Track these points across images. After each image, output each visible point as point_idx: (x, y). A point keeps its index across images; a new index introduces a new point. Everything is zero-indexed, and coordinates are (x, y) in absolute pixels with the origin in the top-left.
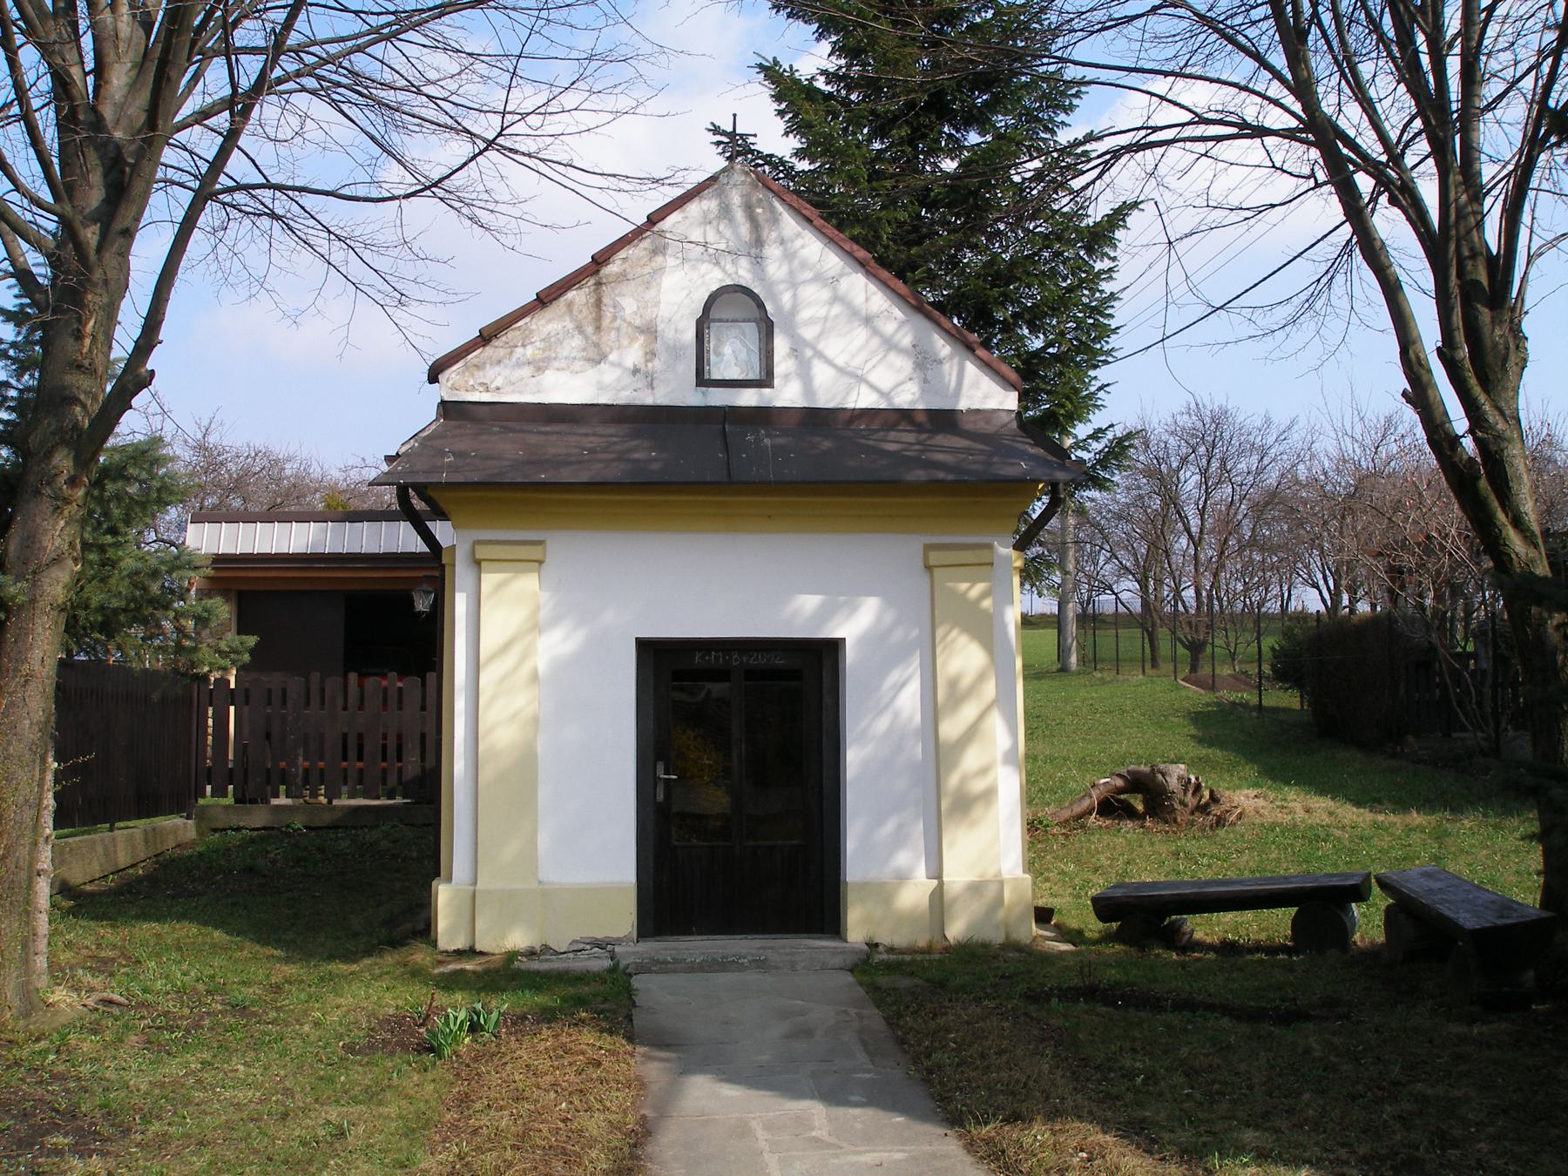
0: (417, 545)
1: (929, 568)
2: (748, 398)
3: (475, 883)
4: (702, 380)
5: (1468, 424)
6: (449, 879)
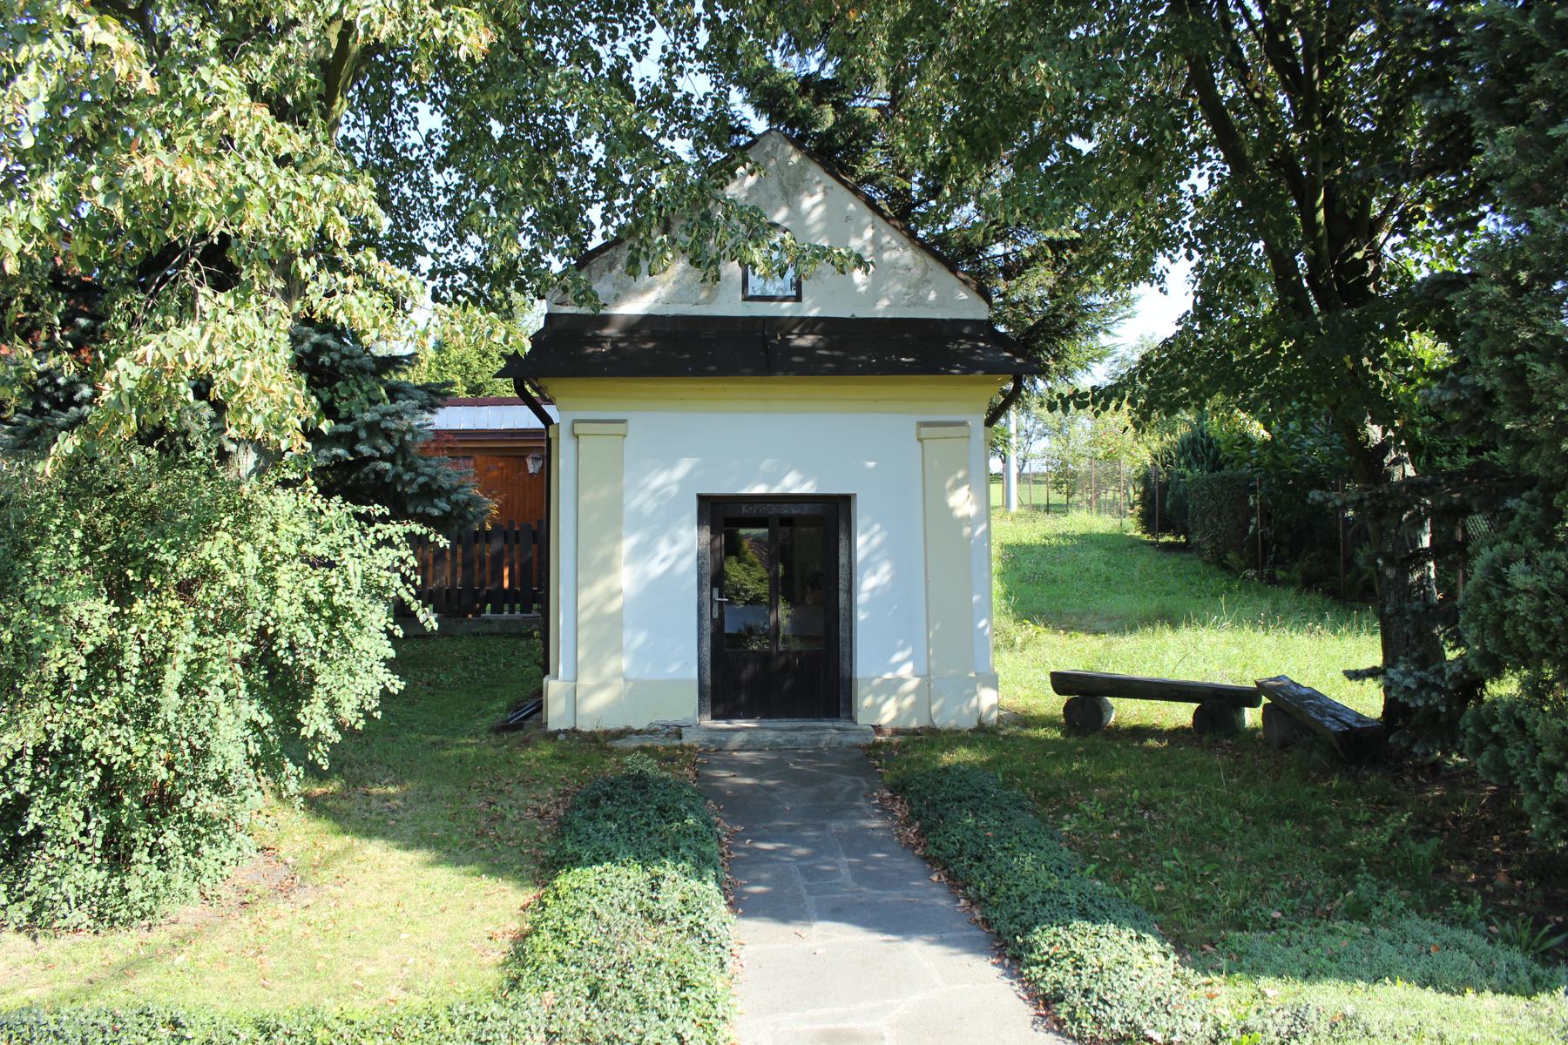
1: (920, 440)
2: (786, 309)
4: (747, 298)
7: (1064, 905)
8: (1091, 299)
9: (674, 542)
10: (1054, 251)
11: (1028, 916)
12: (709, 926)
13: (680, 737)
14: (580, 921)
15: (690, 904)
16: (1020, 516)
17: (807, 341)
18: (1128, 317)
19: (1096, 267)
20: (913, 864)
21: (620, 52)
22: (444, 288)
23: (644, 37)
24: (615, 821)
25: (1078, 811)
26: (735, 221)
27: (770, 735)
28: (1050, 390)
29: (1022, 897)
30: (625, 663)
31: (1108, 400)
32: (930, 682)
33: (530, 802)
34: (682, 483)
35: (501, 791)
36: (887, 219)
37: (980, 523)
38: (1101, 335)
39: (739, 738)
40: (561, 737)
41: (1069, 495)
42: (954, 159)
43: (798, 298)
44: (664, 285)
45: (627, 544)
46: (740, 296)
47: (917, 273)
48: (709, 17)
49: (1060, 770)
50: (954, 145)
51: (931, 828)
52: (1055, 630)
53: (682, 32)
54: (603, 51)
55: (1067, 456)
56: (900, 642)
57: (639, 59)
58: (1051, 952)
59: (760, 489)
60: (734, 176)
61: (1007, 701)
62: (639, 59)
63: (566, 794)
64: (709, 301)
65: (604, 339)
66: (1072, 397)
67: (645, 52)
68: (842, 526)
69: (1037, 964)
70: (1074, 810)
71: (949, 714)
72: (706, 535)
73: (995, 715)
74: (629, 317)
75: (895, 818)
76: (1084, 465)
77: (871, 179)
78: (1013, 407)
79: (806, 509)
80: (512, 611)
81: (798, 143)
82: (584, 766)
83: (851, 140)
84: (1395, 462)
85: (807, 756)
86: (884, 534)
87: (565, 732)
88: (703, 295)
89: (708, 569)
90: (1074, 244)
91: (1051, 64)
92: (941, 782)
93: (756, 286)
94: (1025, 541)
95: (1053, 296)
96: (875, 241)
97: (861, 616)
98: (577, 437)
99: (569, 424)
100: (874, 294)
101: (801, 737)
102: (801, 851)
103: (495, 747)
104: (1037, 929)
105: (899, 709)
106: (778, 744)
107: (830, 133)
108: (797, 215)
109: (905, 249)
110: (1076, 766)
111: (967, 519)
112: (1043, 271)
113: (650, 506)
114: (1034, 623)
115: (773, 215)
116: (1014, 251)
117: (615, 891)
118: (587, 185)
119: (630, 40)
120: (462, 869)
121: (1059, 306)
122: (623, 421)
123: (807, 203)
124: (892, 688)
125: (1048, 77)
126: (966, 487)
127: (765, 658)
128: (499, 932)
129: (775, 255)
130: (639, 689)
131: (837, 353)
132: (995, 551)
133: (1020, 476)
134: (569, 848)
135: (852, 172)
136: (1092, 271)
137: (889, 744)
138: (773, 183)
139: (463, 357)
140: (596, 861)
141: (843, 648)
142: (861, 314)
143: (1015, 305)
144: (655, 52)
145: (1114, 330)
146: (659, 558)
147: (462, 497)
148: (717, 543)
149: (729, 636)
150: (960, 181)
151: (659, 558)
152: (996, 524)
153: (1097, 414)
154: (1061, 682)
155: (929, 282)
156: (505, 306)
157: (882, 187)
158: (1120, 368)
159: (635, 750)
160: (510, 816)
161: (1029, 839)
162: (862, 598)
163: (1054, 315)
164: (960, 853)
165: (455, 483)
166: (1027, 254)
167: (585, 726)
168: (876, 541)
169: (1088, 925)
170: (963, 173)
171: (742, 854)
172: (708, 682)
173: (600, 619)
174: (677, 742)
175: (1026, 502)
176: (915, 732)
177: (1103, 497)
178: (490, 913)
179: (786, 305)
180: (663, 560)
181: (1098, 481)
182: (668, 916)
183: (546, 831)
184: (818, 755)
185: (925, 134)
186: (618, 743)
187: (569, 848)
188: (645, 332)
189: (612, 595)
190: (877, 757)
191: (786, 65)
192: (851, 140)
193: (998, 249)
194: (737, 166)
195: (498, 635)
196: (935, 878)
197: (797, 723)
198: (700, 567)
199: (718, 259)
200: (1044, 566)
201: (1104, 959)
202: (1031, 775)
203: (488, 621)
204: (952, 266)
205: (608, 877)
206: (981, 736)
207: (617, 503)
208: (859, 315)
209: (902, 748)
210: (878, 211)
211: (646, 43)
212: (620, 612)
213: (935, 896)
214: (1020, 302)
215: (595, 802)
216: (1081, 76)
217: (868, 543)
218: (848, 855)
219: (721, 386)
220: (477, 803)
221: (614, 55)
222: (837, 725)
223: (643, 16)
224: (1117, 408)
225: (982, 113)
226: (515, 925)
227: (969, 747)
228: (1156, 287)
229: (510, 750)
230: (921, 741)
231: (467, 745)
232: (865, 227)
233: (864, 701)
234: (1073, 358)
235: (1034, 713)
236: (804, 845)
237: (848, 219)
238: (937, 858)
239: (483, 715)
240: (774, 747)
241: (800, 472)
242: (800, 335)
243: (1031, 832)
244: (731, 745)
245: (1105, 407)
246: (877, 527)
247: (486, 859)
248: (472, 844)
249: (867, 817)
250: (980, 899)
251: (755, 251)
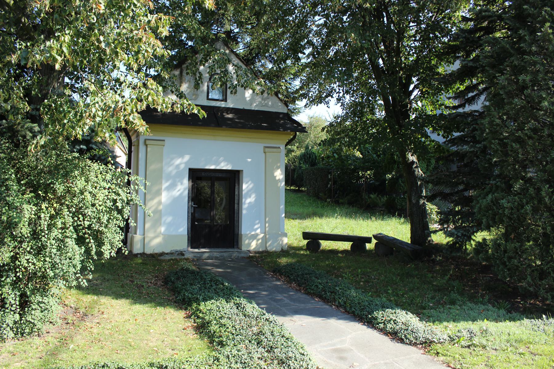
1: (265, 152)
2: (223, 104)
3: (144, 235)
17: (230, 116)
34: (186, 163)
39: (206, 255)
40: (139, 256)
51: (146, 264)
59: (213, 167)
68: (237, 181)
71: (272, 247)
84: (416, 167)
87: (140, 254)
97: (244, 212)
98: (146, 145)
101: (225, 255)
122: (164, 140)
124: (255, 237)
130: (167, 238)
131: (242, 121)
141: (236, 223)
142: (247, 108)
154: (306, 235)
167: (148, 251)
174: (183, 257)
180: (179, 191)
186: (162, 258)
207: (161, 170)
208: (246, 108)
228: (326, 105)
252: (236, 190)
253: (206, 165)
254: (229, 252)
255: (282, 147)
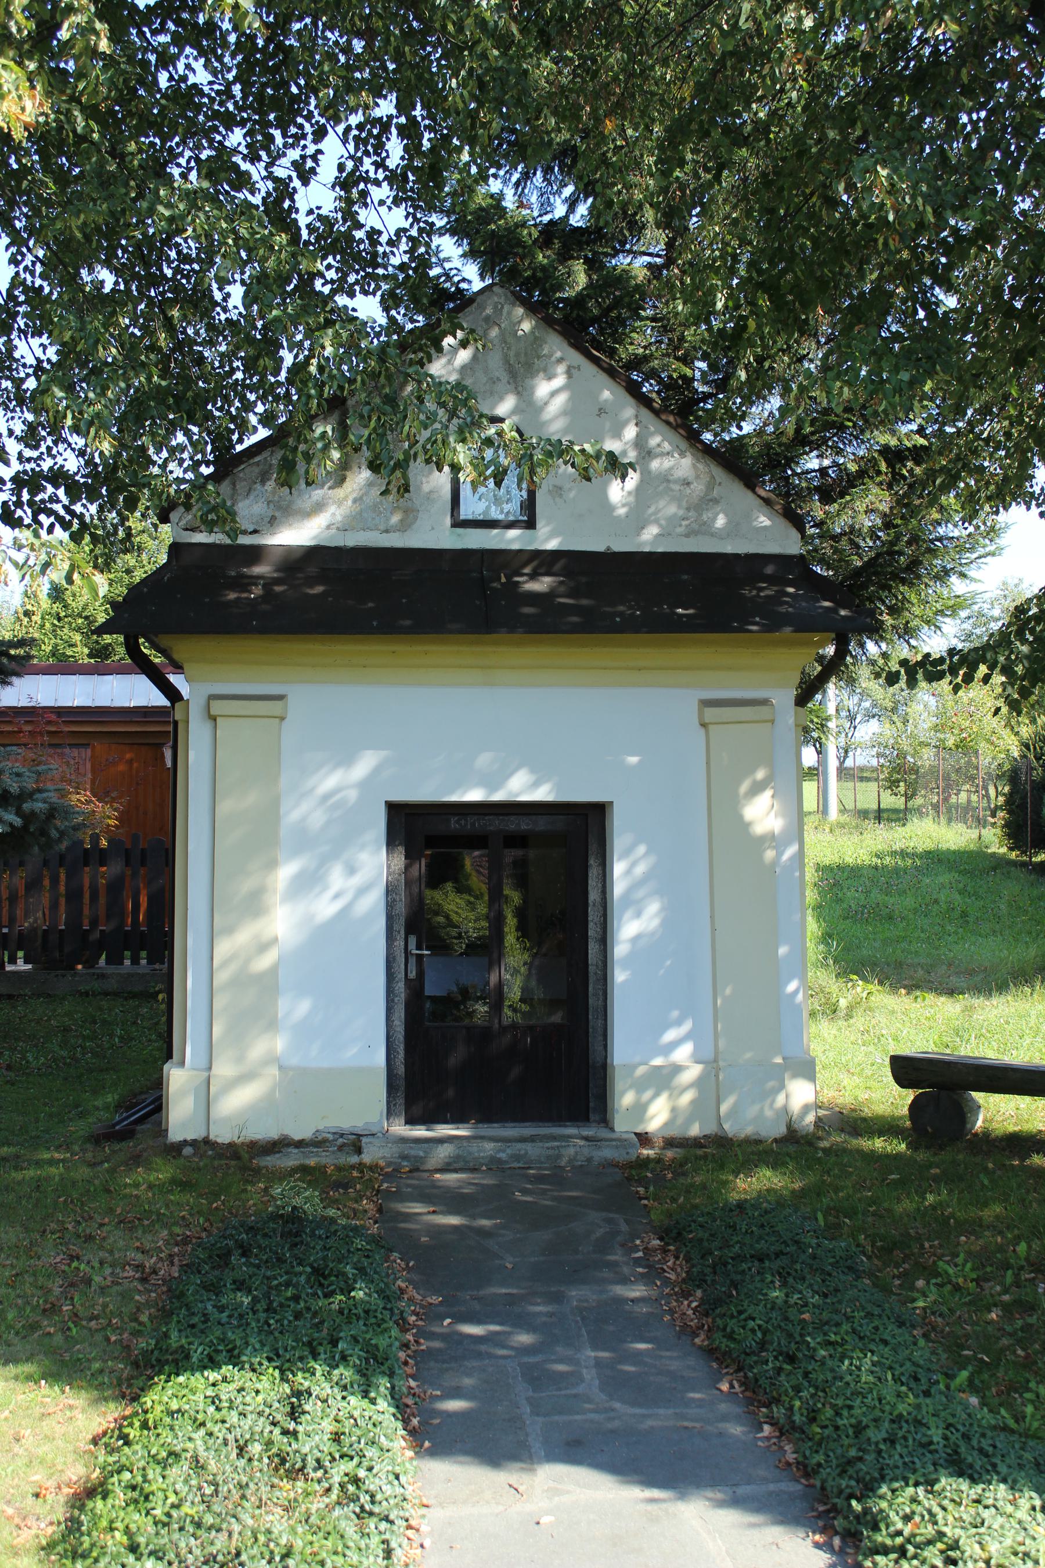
0: (159, 700)
1: (704, 725)
2: (513, 539)
3: (210, 1068)
4: (459, 523)
5: (220, 1140)
6: (182, 1063)
7: (923, 1445)
8: (941, 531)
9: (351, 870)
10: (890, 465)
11: (867, 1467)
12: (371, 1484)
13: (359, 1151)
14: (173, 1472)
15: (346, 1440)
16: (842, 826)
17: (542, 585)
18: (992, 554)
19: (952, 480)
20: (691, 1361)
21: (280, 172)
22: (19, 504)
23: (311, 149)
24: (249, 1291)
25: (938, 1275)
26: (430, 405)
27: (489, 1148)
28: (885, 655)
29: (859, 1429)
30: (280, 1044)
31: (973, 668)
32: (718, 1070)
33: (131, 1254)
34: (365, 785)
35: (89, 1238)
36: (656, 413)
37: (788, 844)
38: (954, 579)
39: (444, 1152)
40: (188, 1151)
41: (908, 797)
42: (752, 324)
43: (530, 524)
44: (340, 503)
45: (286, 872)
46: (448, 521)
47: (698, 488)
48: (403, 120)
49: (906, 1205)
50: (752, 303)
51: (718, 1302)
52: (894, 989)
53: (365, 142)
54: (256, 171)
55: (905, 744)
56: (675, 1014)
57: (306, 182)
58: (907, 1530)
59: (475, 795)
60: (440, 350)
61: (828, 1095)
62: (306, 182)
63: (186, 1241)
64: (404, 526)
65: (254, 580)
66: (921, 664)
67: (313, 171)
68: (593, 847)
69: (885, 1551)
70: (931, 1272)
72: (399, 860)
73: (810, 1118)
74: (289, 549)
75: (666, 1281)
76: (927, 758)
77: (636, 363)
78: (833, 679)
79: (541, 824)
80: (135, 961)
81: (532, 308)
82: (216, 1196)
83: (610, 309)
85: (540, 1179)
86: (652, 860)
87: (194, 1143)
88: (395, 519)
89: (401, 908)
90: (918, 454)
91: (895, 170)
92: (734, 1227)
93: (472, 507)
94: (850, 860)
95: (888, 525)
96: (639, 443)
97: (620, 976)
98: (214, 719)
99: (202, 701)
100: (638, 516)
101: (533, 1150)
102: (524, 1338)
103: (92, 1165)
104: (884, 1489)
105: (674, 1110)
106: (500, 1161)
107: (580, 301)
108: (528, 406)
109: (682, 454)
110: (930, 1198)
111: (770, 839)
112: (875, 490)
113: (318, 819)
114: (864, 979)
115: (494, 406)
116: (835, 464)
117: (233, 1418)
118: (237, 364)
119: (294, 154)
120: (12, 1370)
121: (898, 537)
122: (281, 698)
123: (543, 388)
125: (892, 190)
126: (768, 793)
127: (483, 1036)
128: (51, 1484)
129: (489, 454)
131: (585, 602)
132: (810, 875)
133: (844, 773)
134: (175, 1340)
135: (612, 353)
136: (945, 488)
137: (659, 1160)
138: (495, 361)
139: (85, 607)
140: (213, 1363)
142: (620, 546)
143: (836, 538)
144: (327, 171)
145: (972, 573)
146: (331, 892)
147: (39, 806)
148: (415, 871)
149: (433, 999)
150: (760, 360)
151: (331, 892)
152: (809, 837)
153: (956, 689)
155: (716, 501)
156: (121, 534)
157: (653, 374)
158: (975, 626)
159: (294, 1170)
160: (97, 1279)
161: (867, 1330)
162: (620, 950)
163: (890, 551)
164: (763, 1345)
165: (31, 785)
166: (853, 467)
167: (222, 1135)
168: (640, 869)
169: (964, 1485)
170: (765, 347)
171: (437, 1344)
172: (401, 1070)
173: (242, 980)
174: (354, 1159)
175: (850, 806)
176: (696, 1143)
177: (953, 799)
178: (43, 1450)
179: (513, 533)
180: (337, 896)
181: (947, 778)
182: (311, 1463)
183: (148, 1304)
184: (556, 1177)
185: (712, 292)
186: (270, 1161)
187: (175, 1340)
188: (312, 570)
189: (263, 947)
190: (643, 1181)
191: (521, 205)
192: (610, 309)
193: (812, 462)
194: (444, 334)
195: (116, 994)
196: (725, 1387)
197: (527, 1130)
198: (390, 906)
199: (407, 460)
200: (876, 896)
201: (993, 1547)
202: (865, 1212)
203: (102, 976)
204: (750, 482)
205: (226, 1392)
206: (792, 1149)
207: (271, 813)
209: (679, 1167)
210: (644, 401)
211: (314, 158)
212: (274, 970)
213: (725, 1418)
214: (843, 534)
215: (225, 1256)
216: (938, 190)
217: (628, 872)
218: (595, 1347)
219: (419, 648)
220: (52, 1256)
221: (271, 176)
222: (586, 1132)
223: (309, 117)
224: (986, 679)
225: (791, 258)
226: (77, 1472)
227: (774, 1167)
229: (112, 1171)
230: (705, 1157)
231: (52, 1162)
232: (624, 424)
233: (625, 1099)
234: (917, 610)
235: (867, 1112)
236: (531, 1328)
237: (601, 411)
238: (728, 1353)
239: (82, 1115)
240: (495, 1165)
241: (532, 771)
242: (534, 576)
243: (869, 1315)
244: (432, 1163)
245: (968, 679)
246: (642, 849)
247: (52, 1352)
248: (34, 1327)
249: (624, 1281)
250: (794, 1427)
251: (460, 447)
252: (592, 883)
253: (452, 792)
254: (554, 1138)
255: (784, 697)
